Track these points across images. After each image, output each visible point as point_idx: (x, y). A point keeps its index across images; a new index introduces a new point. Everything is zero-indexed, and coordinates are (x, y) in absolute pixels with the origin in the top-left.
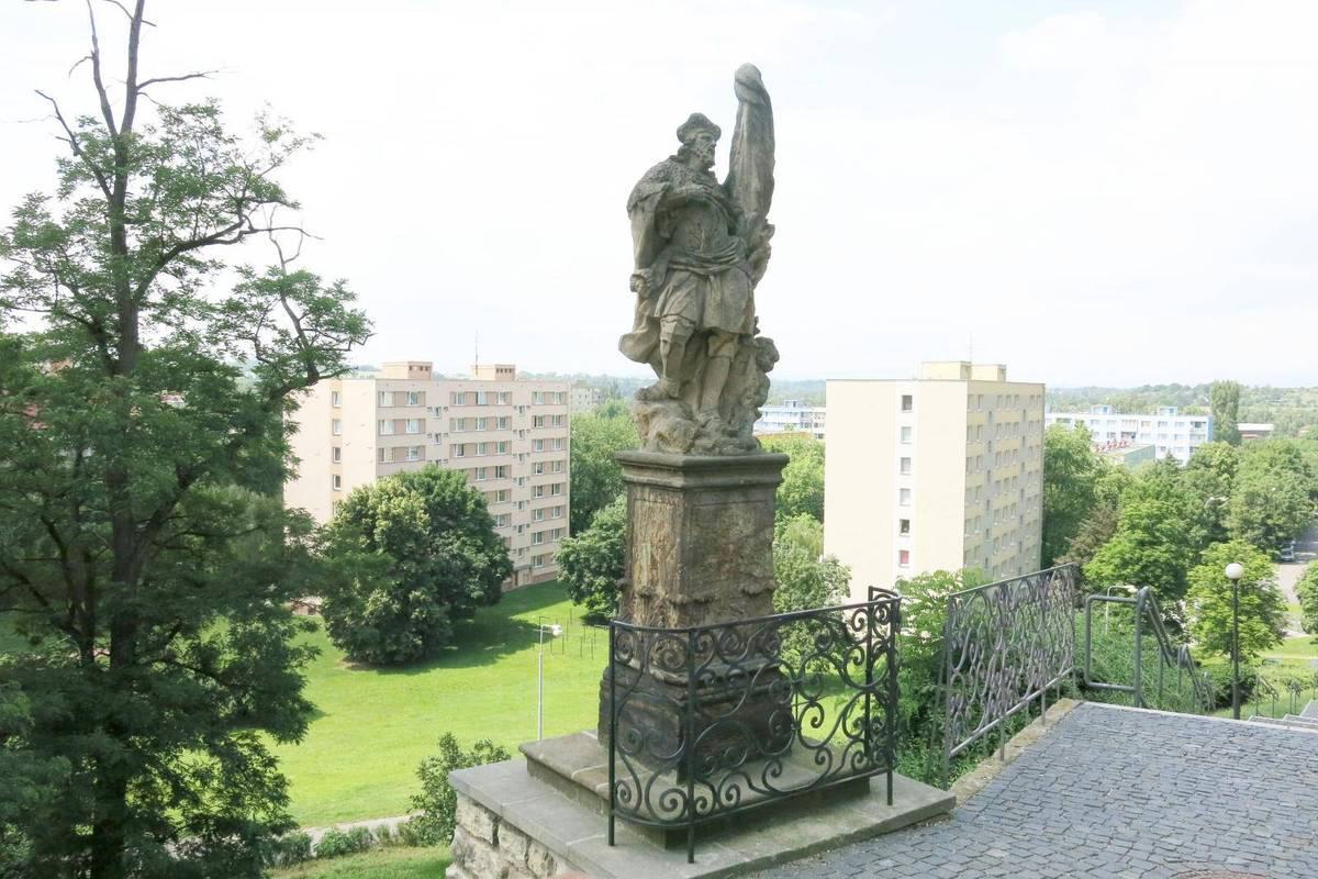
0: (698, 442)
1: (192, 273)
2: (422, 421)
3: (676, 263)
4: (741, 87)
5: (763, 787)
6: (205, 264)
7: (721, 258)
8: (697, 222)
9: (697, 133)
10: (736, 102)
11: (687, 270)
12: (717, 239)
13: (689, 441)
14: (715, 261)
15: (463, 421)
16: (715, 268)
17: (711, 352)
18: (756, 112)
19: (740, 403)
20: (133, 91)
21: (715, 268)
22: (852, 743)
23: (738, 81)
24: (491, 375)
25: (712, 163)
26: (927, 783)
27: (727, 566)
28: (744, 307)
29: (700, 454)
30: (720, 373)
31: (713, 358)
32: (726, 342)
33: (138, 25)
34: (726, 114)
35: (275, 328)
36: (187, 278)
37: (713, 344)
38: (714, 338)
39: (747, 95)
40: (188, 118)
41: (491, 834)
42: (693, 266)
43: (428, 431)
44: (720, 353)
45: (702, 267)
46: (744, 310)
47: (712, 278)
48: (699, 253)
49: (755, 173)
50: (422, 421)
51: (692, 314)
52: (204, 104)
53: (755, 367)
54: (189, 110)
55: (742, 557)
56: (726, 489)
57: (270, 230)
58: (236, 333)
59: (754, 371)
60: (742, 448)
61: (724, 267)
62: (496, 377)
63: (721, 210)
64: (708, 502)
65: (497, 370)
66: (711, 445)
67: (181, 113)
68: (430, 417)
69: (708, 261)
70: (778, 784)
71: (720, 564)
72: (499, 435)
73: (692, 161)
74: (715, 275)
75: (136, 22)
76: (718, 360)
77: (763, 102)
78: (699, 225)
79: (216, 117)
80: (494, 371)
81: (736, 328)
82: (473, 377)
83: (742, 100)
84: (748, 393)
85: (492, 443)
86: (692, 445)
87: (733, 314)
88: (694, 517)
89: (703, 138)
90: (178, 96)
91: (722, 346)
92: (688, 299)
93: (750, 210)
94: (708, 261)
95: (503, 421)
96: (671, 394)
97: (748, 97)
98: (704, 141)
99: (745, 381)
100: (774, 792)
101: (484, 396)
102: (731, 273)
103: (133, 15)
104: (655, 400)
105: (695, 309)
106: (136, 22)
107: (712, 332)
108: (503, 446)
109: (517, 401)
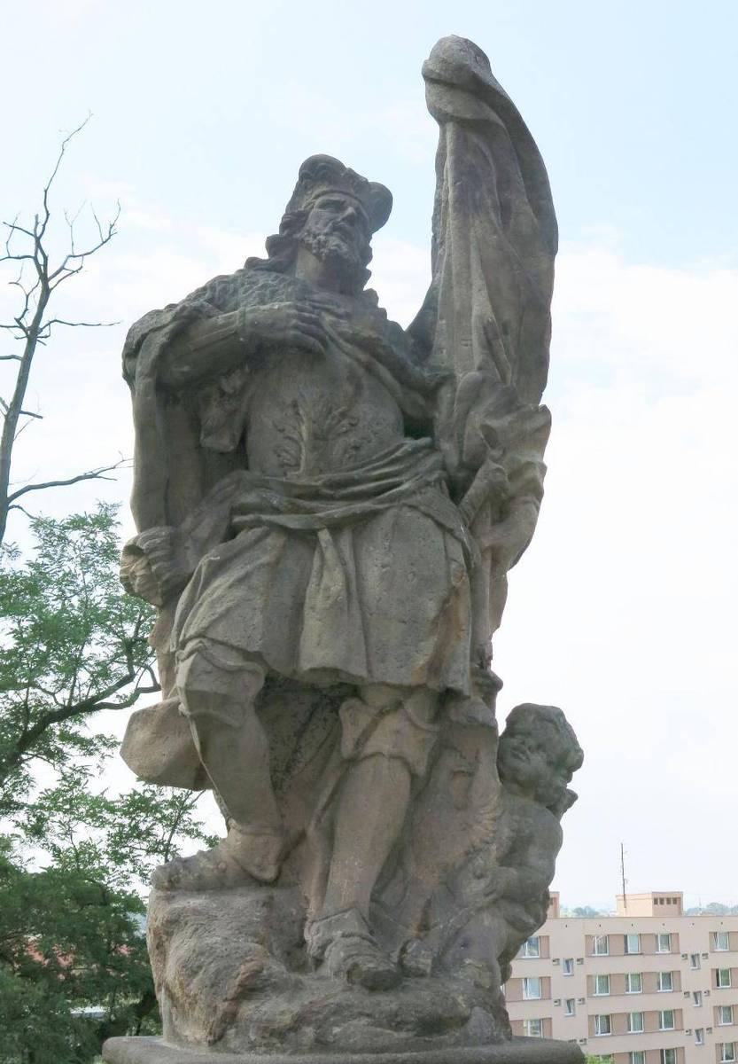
0: (247, 1009)
1: (75, 756)
2: (545, 981)
3: (243, 510)
4: (438, 89)
6: (90, 742)
8: (289, 401)
9: (335, 204)
10: (432, 129)
11: (258, 523)
12: (352, 439)
13: (223, 1006)
14: (338, 489)
15: (605, 980)
16: (338, 510)
17: (347, 747)
18: (474, 139)
19: (450, 887)
21: (338, 510)
23: (431, 78)
24: (647, 909)
25: (252, 263)
28: (432, 614)
29: (252, 1047)
30: (374, 804)
31: (353, 761)
32: (382, 713)
33: (16, 418)
34: (405, 154)
35: (199, 835)
36: (69, 763)
37: (353, 720)
38: (353, 702)
39: (458, 104)
40: (74, 535)
42: (277, 511)
43: (555, 997)
44: (370, 748)
45: (296, 510)
46: (435, 622)
47: (324, 536)
48: (300, 477)
49: (478, 281)
50: (545, 981)
51: (252, 630)
52: (94, 511)
53: (496, 783)
54: (78, 523)
58: (145, 845)
59: (494, 798)
60: (398, 1026)
61: (367, 505)
62: (654, 909)
63: (369, 369)
65: (655, 902)
66: (287, 1019)
67: (65, 528)
68: (557, 973)
69: (315, 495)
72: (665, 1001)
73: (299, 263)
74: (336, 528)
76: (367, 767)
77: (494, 117)
78: (295, 405)
79: (111, 529)
80: (651, 901)
81: (408, 667)
82: (622, 913)
83: (442, 118)
84: (480, 862)
85: (656, 1011)
86: (230, 1019)
89: (322, 206)
90: (58, 506)
91: (375, 724)
92: (239, 593)
93: (466, 369)
94: (315, 495)
95: (668, 978)
96: (255, 872)
97: (449, 109)
98: (326, 214)
99: (466, 827)
101: (636, 939)
102: (386, 521)
103: (8, 404)
104: (200, 888)
105: (258, 619)
107: (339, 691)
108: (670, 1018)
109: (687, 947)
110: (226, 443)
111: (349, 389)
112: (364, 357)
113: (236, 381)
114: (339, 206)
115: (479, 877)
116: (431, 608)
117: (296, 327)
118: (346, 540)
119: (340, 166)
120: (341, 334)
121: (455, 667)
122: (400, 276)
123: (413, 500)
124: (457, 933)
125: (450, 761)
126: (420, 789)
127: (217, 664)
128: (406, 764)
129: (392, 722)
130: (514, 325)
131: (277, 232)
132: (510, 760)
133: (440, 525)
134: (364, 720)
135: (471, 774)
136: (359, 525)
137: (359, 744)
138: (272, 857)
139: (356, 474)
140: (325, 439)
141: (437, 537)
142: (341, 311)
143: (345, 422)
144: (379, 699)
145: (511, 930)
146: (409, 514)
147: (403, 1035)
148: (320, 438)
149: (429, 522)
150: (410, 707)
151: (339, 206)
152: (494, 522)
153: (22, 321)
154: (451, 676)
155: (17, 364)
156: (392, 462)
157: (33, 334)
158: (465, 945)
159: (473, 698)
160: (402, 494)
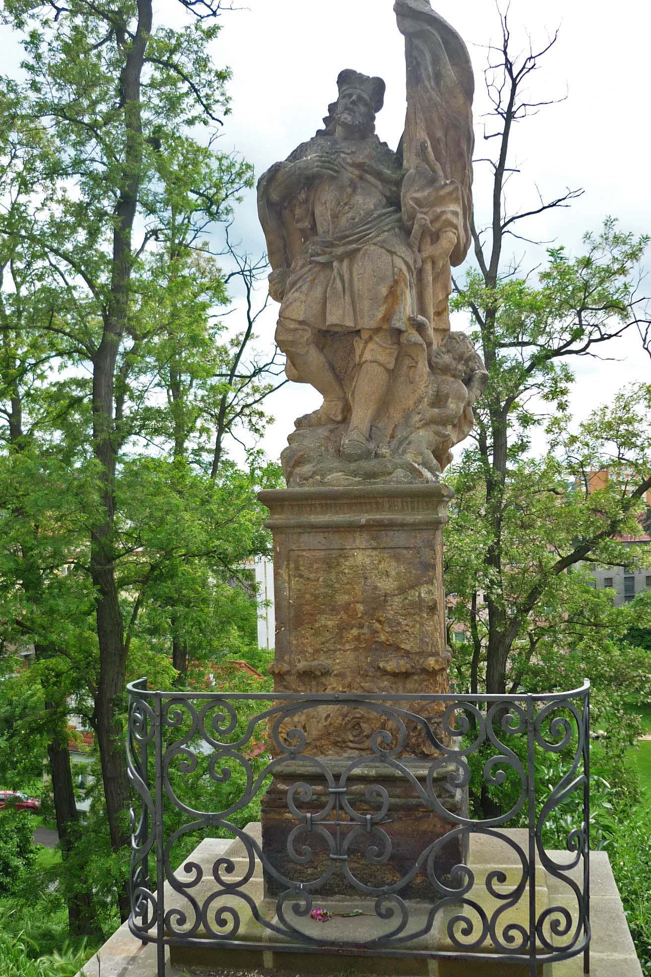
0: (297, 470)
5: (275, 921)
7: (348, 236)
9: (358, 94)
19: (407, 417)
20: (498, 231)
21: (340, 250)
22: (240, 884)
25: (319, 132)
26: (105, 941)
27: (355, 632)
32: (366, 343)
41: (246, 892)
45: (325, 253)
55: (379, 621)
56: (351, 528)
57: (636, 322)
61: (354, 246)
64: (312, 545)
70: (312, 930)
71: (342, 628)
75: (500, 170)
87: (366, 305)
88: (292, 565)
100: (295, 934)
106: (500, 170)
110: (307, 224)
111: (349, 190)
112: (357, 172)
113: (303, 196)
114: (350, 95)
115: (419, 413)
116: (384, 291)
117: (317, 166)
118: (345, 263)
119: (354, 72)
120: (347, 163)
121: (395, 318)
122: (390, 125)
123: (374, 241)
124: (406, 438)
125: (407, 362)
126: (392, 374)
127: (616, 309)
128: (380, 364)
129: (371, 346)
130: (443, 139)
131: (328, 114)
132: (434, 359)
133: (388, 251)
134: (361, 346)
135: (415, 367)
136: (351, 255)
137: (361, 357)
138: (339, 411)
139: (347, 233)
140: (337, 217)
141: (387, 258)
142: (348, 151)
143: (347, 207)
144: (365, 335)
145: (437, 437)
146: (373, 247)
147: (357, 479)
148: (335, 217)
149: (383, 251)
150: (376, 339)
151: (350, 95)
152: (432, 244)
153: (499, 110)
154: (393, 322)
155: (501, 137)
156: (367, 224)
157: (509, 116)
158: (409, 444)
159: (410, 331)
160: (372, 238)
